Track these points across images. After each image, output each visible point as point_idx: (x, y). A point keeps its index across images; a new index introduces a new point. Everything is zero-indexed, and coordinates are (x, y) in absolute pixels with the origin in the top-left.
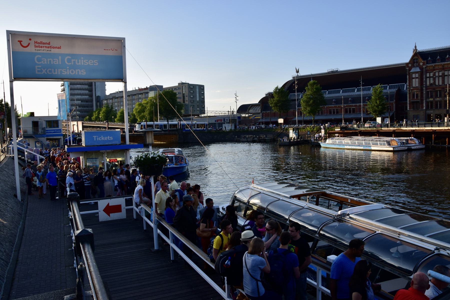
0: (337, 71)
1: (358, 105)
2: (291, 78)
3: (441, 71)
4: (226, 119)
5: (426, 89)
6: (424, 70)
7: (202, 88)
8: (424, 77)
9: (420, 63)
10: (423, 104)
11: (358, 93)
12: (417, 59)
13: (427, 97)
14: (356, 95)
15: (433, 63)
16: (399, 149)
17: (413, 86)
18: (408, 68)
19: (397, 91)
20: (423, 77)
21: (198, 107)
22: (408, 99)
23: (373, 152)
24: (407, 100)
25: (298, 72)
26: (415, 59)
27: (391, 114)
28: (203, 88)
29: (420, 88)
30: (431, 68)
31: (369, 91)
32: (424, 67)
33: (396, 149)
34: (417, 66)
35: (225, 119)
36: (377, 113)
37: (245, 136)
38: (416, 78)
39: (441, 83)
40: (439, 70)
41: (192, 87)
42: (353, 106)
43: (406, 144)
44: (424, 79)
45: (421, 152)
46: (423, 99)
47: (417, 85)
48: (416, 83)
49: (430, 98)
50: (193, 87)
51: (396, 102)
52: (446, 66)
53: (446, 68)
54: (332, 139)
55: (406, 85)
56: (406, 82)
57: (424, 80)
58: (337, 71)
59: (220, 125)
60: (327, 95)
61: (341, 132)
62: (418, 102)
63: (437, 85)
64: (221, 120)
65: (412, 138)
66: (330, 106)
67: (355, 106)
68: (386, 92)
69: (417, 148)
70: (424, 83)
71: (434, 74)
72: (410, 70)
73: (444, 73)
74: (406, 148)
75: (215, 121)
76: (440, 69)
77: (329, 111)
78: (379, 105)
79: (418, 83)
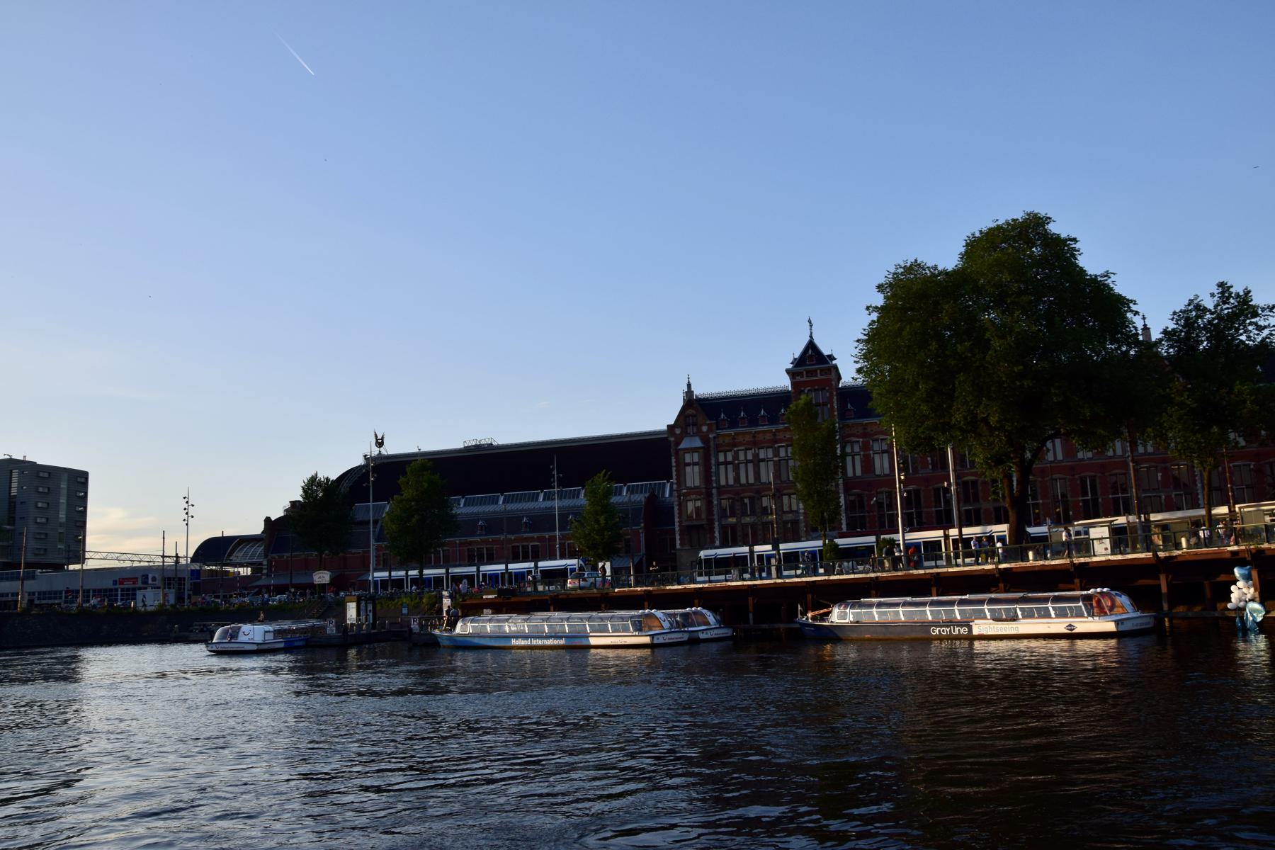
0: (491, 444)
1: (547, 537)
2: (360, 461)
3: (751, 449)
4: (150, 576)
5: (719, 494)
6: (712, 444)
7: (79, 480)
8: (713, 462)
9: (701, 426)
10: (714, 532)
11: (548, 504)
12: (693, 416)
13: (723, 515)
14: (540, 509)
16: (667, 641)
17: (687, 485)
19: (648, 499)
20: (711, 464)
21: (60, 540)
22: (677, 520)
23: (593, 651)
24: (673, 524)
25: (380, 444)
26: (688, 416)
27: (636, 559)
28: (83, 480)
29: (704, 490)
31: (575, 500)
33: (658, 639)
34: (695, 435)
35: (147, 576)
37: (204, 625)
38: (695, 464)
39: (751, 480)
40: (747, 446)
41: (46, 475)
42: (533, 539)
43: (684, 626)
44: (714, 467)
46: (713, 520)
47: (697, 483)
48: (693, 477)
50: (49, 473)
52: (760, 437)
54: (472, 621)
56: (669, 478)
58: (491, 444)
59: (128, 595)
60: (462, 508)
61: (500, 600)
63: (744, 484)
64: (135, 580)
66: (470, 539)
67: (539, 539)
68: (621, 501)
69: (714, 636)
70: (714, 478)
71: (736, 457)
72: (678, 444)
73: (758, 455)
74: (686, 637)
75: (115, 582)
77: (466, 553)
79: (700, 479)
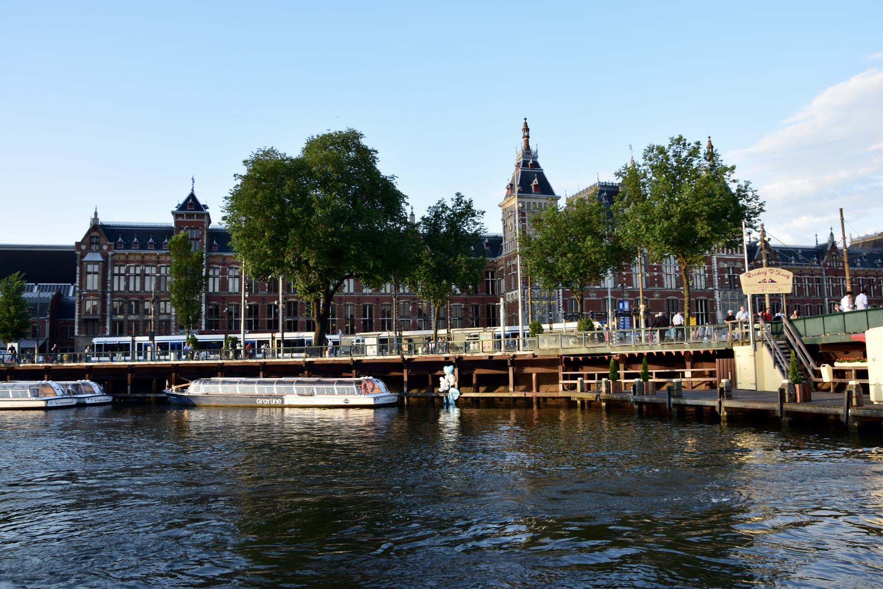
6: (110, 259)
8: (110, 272)
12: (97, 237)
15: (126, 248)
18: (79, 253)
19: (54, 297)
22: (77, 314)
24: (74, 317)
26: (93, 237)
27: (41, 343)
29: (100, 293)
30: (122, 258)
32: (110, 253)
34: (97, 251)
36: (10, 334)
38: (95, 273)
39: (138, 289)
45: (107, 407)
47: (96, 288)
48: (93, 282)
49: (119, 314)
51: (50, 319)
52: (147, 258)
53: (148, 261)
55: (72, 288)
57: (109, 278)
62: (96, 320)
65: (88, 381)
70: (109, 285)
71: (128, 271)
72: (83, 256)
74: (74, 402)
76: (138, 261)
78: (15, 317)
